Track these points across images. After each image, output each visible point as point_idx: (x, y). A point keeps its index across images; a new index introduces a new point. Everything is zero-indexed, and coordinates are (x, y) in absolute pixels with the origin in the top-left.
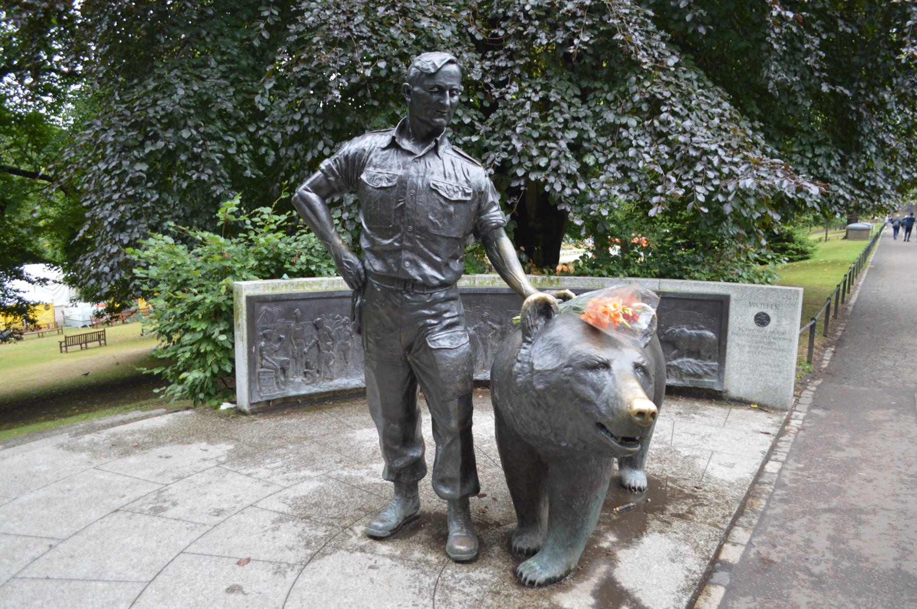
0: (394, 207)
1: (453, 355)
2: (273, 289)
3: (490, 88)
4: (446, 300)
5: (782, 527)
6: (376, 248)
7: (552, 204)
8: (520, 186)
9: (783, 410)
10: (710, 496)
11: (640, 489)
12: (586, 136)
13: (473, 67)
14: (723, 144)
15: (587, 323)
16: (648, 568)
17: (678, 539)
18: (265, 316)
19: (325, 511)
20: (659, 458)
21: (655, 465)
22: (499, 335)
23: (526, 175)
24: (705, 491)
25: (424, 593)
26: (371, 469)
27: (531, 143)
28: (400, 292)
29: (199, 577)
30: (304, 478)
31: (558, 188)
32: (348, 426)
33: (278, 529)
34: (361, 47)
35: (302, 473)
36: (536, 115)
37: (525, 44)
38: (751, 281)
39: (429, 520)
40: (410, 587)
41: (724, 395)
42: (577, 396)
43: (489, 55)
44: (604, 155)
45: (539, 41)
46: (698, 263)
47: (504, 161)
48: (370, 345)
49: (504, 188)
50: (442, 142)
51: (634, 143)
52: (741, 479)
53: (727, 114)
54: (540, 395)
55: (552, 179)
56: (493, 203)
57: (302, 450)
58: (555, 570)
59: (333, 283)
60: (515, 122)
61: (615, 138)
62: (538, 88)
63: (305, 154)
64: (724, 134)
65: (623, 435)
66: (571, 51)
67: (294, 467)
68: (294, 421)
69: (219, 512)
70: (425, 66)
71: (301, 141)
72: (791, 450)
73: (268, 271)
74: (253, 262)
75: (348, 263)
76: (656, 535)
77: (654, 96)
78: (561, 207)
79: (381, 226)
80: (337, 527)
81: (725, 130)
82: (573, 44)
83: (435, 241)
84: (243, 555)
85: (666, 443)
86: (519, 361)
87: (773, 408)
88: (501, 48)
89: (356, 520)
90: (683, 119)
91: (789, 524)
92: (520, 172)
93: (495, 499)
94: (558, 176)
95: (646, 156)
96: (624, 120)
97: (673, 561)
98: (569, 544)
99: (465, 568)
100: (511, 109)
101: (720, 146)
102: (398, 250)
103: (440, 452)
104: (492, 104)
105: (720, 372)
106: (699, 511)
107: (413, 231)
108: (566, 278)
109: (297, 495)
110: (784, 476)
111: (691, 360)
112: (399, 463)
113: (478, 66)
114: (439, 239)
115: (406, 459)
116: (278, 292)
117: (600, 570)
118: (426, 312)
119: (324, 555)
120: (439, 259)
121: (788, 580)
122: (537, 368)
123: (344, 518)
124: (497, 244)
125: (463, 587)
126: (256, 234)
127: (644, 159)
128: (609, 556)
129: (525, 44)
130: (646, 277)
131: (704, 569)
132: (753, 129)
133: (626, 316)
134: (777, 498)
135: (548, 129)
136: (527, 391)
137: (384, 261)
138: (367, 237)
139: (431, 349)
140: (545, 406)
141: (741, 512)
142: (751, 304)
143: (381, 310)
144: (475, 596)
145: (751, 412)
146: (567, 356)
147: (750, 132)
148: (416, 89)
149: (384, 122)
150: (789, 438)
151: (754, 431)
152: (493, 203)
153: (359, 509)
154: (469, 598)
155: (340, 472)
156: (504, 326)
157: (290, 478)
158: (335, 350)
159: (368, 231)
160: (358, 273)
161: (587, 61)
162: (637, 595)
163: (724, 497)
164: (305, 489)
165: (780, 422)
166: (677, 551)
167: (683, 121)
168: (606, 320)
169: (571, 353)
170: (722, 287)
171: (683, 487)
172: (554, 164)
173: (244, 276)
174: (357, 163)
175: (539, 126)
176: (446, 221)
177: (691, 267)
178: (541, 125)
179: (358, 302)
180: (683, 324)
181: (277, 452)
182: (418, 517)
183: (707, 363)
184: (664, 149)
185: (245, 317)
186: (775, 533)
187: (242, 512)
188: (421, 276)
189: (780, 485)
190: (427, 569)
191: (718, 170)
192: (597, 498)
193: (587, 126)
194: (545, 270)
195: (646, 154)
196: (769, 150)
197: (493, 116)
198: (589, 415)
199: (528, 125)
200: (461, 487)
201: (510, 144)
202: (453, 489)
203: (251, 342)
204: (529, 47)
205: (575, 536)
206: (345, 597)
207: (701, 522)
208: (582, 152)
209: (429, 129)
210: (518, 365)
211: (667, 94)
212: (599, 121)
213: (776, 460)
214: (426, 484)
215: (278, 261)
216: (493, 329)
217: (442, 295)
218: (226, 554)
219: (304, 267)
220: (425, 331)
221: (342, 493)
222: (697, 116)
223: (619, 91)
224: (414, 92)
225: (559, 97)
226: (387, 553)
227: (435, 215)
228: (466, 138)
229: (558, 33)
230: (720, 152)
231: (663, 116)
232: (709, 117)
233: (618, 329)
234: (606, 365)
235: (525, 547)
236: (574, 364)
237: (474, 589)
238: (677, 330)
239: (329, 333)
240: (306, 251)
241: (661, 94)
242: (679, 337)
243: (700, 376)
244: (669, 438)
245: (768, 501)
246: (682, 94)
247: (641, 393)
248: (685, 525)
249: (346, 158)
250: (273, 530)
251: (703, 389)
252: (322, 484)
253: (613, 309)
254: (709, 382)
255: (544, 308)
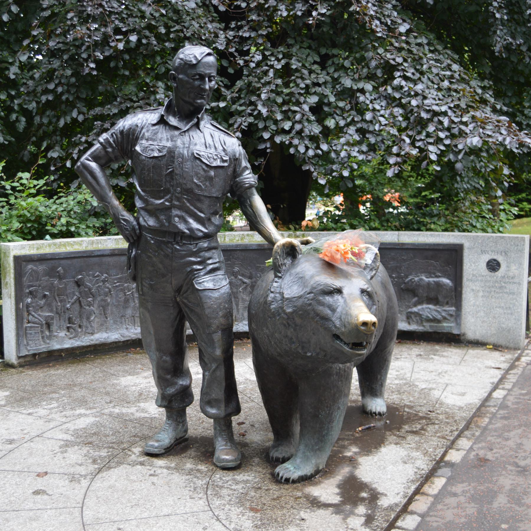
0: (165, 173)
1: (216, 294)
2: (38, 249)
3: (235, 57)
4: (209, 249)
5: (499, 436)
6: (149, 207)
7: (298, 165)
8: (266, 148)
9: (516, 349)
10: (441, 417)
11: (380, 414)
12: (326, 101)
13: (218, 37)
14: (452, 105)
15: (324, 260)
16: (384, 468)
17: (411, 448)
18: (31, 275)
19: (104, 439)
20: (398, 391)
21: (395, 396)
22: (249, 289)
23: (271, 139)
24: (438, 414)
25: (198, 490)
26: (139, 407)
27: (275, 108)
28: (171, 243)
29: (7, 485)
30: (80, 416)
31: (302, 149)
32: (113, 375)
33: (66, 452)
34: (113, 22)
35: (78, 412)
36: (279, 81)
37: (267, 16)
38: (484, 230)
39: (198, 443)
40: (186, 487)
41: (462, 338)
42: (318, 315)
43: (233, 25)
44: (344, 118)
45: (279, 13)
46: (435, 216)
47: (250, 124)
48: (145, 289)
49: (251, 150)
50: (202, 118)
51: (370, 106)
52: (470, 404)
53: (456, 75)
54: (290, 316)
55: (296, 141)
56: (246, 168)
57: (73, 394)
58: (307, 470)
59: (92, 243)
60: (259, 89)
61: (353, 102)
62: (280, 56)
63: (58, 120)
64: (454, 94)
65: (353, 341)
66: (310, 22)
67: (68, 407)
68: (59, 371)
69: (11, 442)
70: (188, 59)
71: (53, 108)
72: (517, 381)
73: (30, 233)
74: (16, 225)
75: (125, 220)
76: (393, 446)
77: (387, 62)
78: (305, 168)
79: (154, 188)
80: (117, 449)
81: (456, 91)
82: (311, 16)
83: (199, 200)
84: (40, 470)
85: (406, 379)
86: (272, 292)
87: (507, 348)
88: (243, 19)
89: (133, 444)
90: (415, 82)
91: (506, 434)
92: (266, 136)
93: (253, 426)
94: (302, 138)
95: (381, 119)
96: (360, 85)
97: (405, 463)
98: (317, 447)
99: (231, 473)
100: (255, 76)
101: (450, 108)
102: (169, 208)
103: (207, 377)
104: (236, 71)
105: (457, 316)
106: (430, 428)
107: (180, 193)
108: (311, 233)
109: (76, 427)
110: (508, 400)
111: (431, 306)
112: (171, 390)
113: (222, 35)
114: (202, 198)
115: (177, 387)
116: (42, 252)
117: (345, 471)
118: (193, 259)
119: (110, 468)
120: (202, 215)
121: (499, 471)
122: (286, 296)
123: (122, 443)
124: (250, 202)
125: (230, 485)
126: (16, 198)
127: (380, 122)
128: (352, 461)
129: (267, 16)
130: (386, 230)
131: (430, 467)
132: (483, 88)
133: (354, 254)
134: (499, 416)
135: (291, 94)
136: (279, 315)
137: (157, 218)
138: (141, 197)
139: (198, 290)
140: (293, 326)
141: (467, 427)
142: (483, 252)
143: (154, 259)
144: (241, 491)
145: (486, 352)
146: (310, 285)
147: (480, 91)
148: (181, 76)
149: (135, 89)
150: (518, 371)
151: (487, 367)
152: (246, 168)
153: (134, 436)
154: (236, 492)
155: (112, 410)
156: (254, 280)
157: (67, 415)
158: (96, 306)
159: (142, 193)
160: (134, 229)
161: (325, 30)
162: (374, 486)
163: (453, 417)
164: (82, 423)
165: (512, 359)
166: (409, 456)
167: (416, 84)
168: (338, 256)
169: (312, 283)
170: (456, 237)
171: (419, 412)
172: (298, 127)
173: (9, 238)
174: (130, 137)
175: (282, 92)
176: (207, 184)
177: (428, 220)
178: (284, 91)
179: (134, 253)
180: (422, 273)
181: (51, 396)
182: (187, 440)
183: (444, 308)
184: (398, 111)
185: (12, 276)
186: (493, 440)
187: (31, 440)
188: (188, 229)
189: (503, 406)
190: (198, 475)
191: (449, 129)
192: (339, 408)
193: (327, 91)
194: (291, 226)
195: (383, 117)
196: (498, 107)
197: (239, 84)
198: (327, 329)
199: (272, 91)
200: (226, 406)
201: (256, 109)
202: (219, 408)
203: (18, 299)
204: (270, 19)
205: (322, 441)
206: (133, 495)
207: (431, 436)
208: (323, 116)
209: (192, 108)
210: (272, 295)
211: (400, 60)
212: (337, 86)
213: (503, 389)
214: (193, 411)
215: (40, 224)
216: (244, 283)
217: (206, 245)
218: (26, 470)
219: (64, 229)
220: (192, 275)
221: (117, 425)
222: (429, 78)
223: (355, 58)
224: (179, 79)
225: (300, 64)
226: (164, 465)
227: (199, 179)
228: (214, 104)
229: (297, 5)
230: (450, 113)
231: (396, 82)
232: (440, 78)
233: (348, 264)
234: (339, 291)
235: (281, 456)
236: (314, 291)
237: (239, 487)
238: (416, 279)
239: (90, 289)
240: (65, 213)
241: (394, 60)
242: (419, 285)
243: (439, 321)
244: (408, 375)
245: (491, 419)
246: (414, 60)
247: (366, 310)
248: (417, 438)
249: (122, 132)
250: (62, 452)
251: (443, 333)
252: (97, 419)
253: (343, 248)
254: (448, 326)
255: (291, 250)
